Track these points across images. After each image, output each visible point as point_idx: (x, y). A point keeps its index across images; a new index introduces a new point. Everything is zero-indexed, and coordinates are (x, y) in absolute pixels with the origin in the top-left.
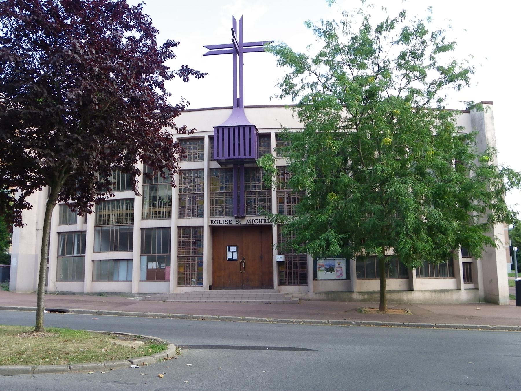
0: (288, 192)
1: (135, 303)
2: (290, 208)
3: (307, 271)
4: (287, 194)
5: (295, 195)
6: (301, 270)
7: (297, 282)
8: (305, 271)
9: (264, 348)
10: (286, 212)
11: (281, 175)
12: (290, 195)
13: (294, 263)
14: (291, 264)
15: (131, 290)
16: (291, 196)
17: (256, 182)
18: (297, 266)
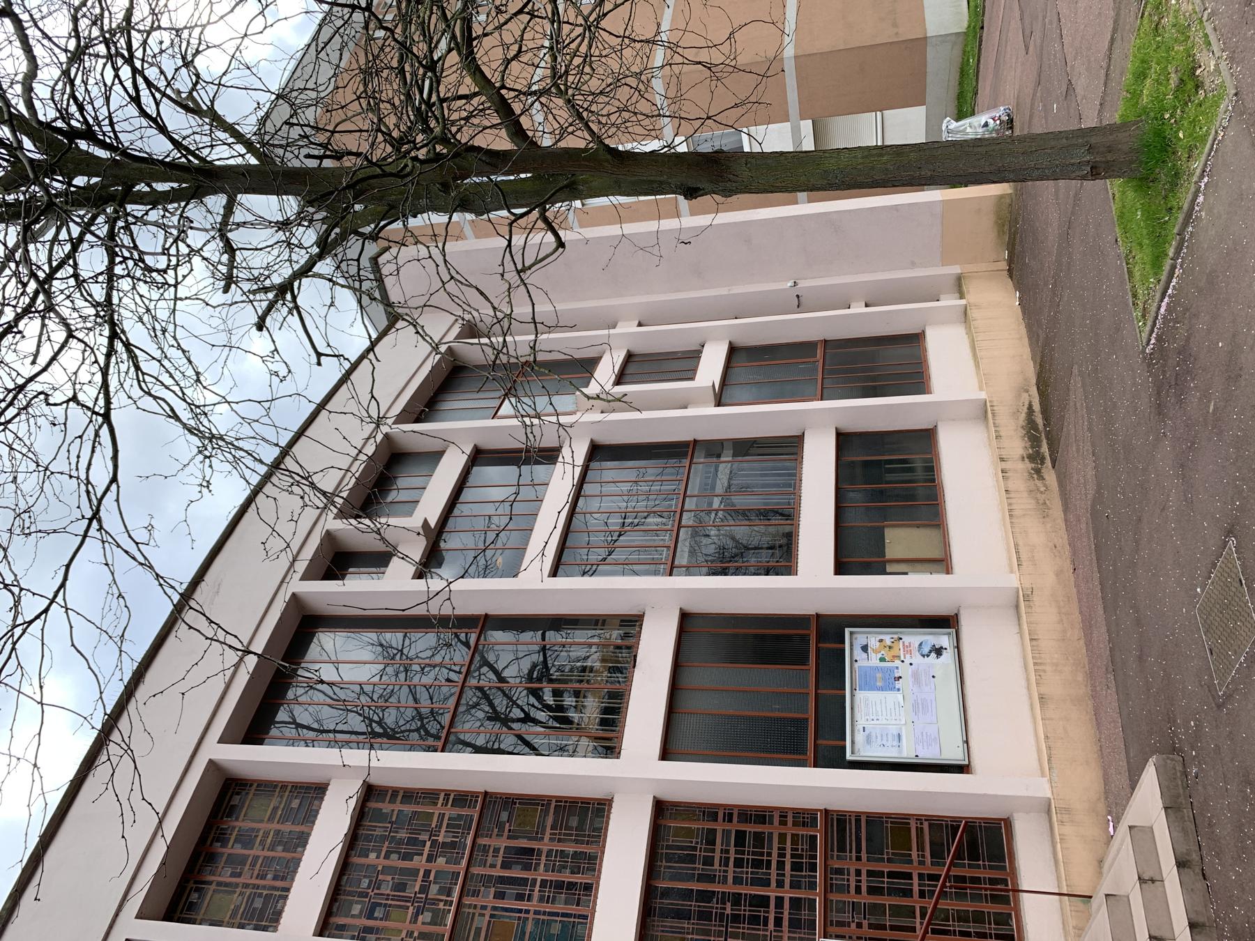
0: (471, 886)
1: (1019, 620)
2: (559, 885)
3: (919, 818)
4: (476, 893)
5: (497, 850)
6: (914, 853)
7: (993, 881)
8: (920, 831)
9: (787, 454)
10: (572, 909)
11: (370, 916)
12: (488, 880)
13: (872, 891)
14: (876, 909)
15: (926, 34)
16: (498, 872)
17: (746, 857)
18: (892, 875)
